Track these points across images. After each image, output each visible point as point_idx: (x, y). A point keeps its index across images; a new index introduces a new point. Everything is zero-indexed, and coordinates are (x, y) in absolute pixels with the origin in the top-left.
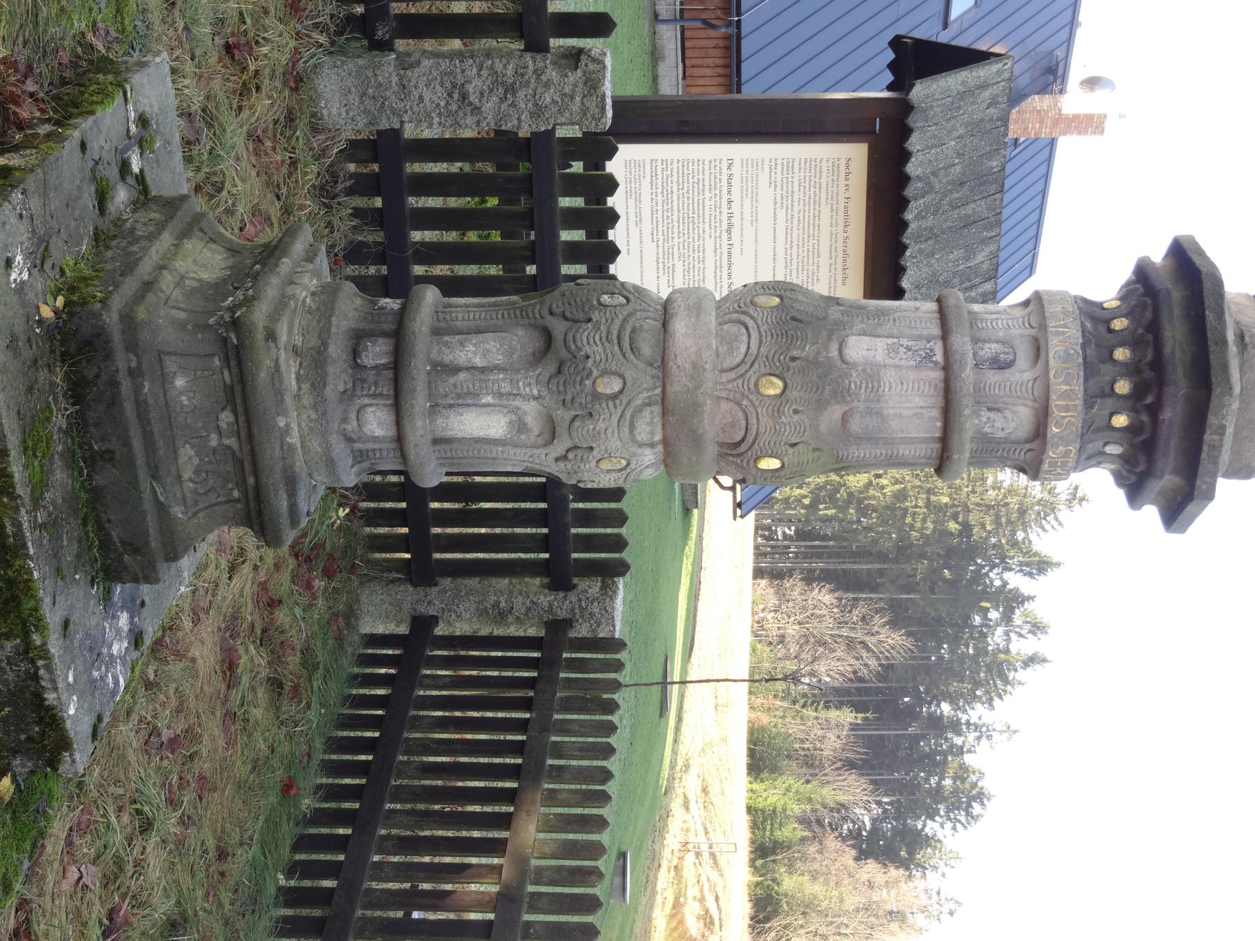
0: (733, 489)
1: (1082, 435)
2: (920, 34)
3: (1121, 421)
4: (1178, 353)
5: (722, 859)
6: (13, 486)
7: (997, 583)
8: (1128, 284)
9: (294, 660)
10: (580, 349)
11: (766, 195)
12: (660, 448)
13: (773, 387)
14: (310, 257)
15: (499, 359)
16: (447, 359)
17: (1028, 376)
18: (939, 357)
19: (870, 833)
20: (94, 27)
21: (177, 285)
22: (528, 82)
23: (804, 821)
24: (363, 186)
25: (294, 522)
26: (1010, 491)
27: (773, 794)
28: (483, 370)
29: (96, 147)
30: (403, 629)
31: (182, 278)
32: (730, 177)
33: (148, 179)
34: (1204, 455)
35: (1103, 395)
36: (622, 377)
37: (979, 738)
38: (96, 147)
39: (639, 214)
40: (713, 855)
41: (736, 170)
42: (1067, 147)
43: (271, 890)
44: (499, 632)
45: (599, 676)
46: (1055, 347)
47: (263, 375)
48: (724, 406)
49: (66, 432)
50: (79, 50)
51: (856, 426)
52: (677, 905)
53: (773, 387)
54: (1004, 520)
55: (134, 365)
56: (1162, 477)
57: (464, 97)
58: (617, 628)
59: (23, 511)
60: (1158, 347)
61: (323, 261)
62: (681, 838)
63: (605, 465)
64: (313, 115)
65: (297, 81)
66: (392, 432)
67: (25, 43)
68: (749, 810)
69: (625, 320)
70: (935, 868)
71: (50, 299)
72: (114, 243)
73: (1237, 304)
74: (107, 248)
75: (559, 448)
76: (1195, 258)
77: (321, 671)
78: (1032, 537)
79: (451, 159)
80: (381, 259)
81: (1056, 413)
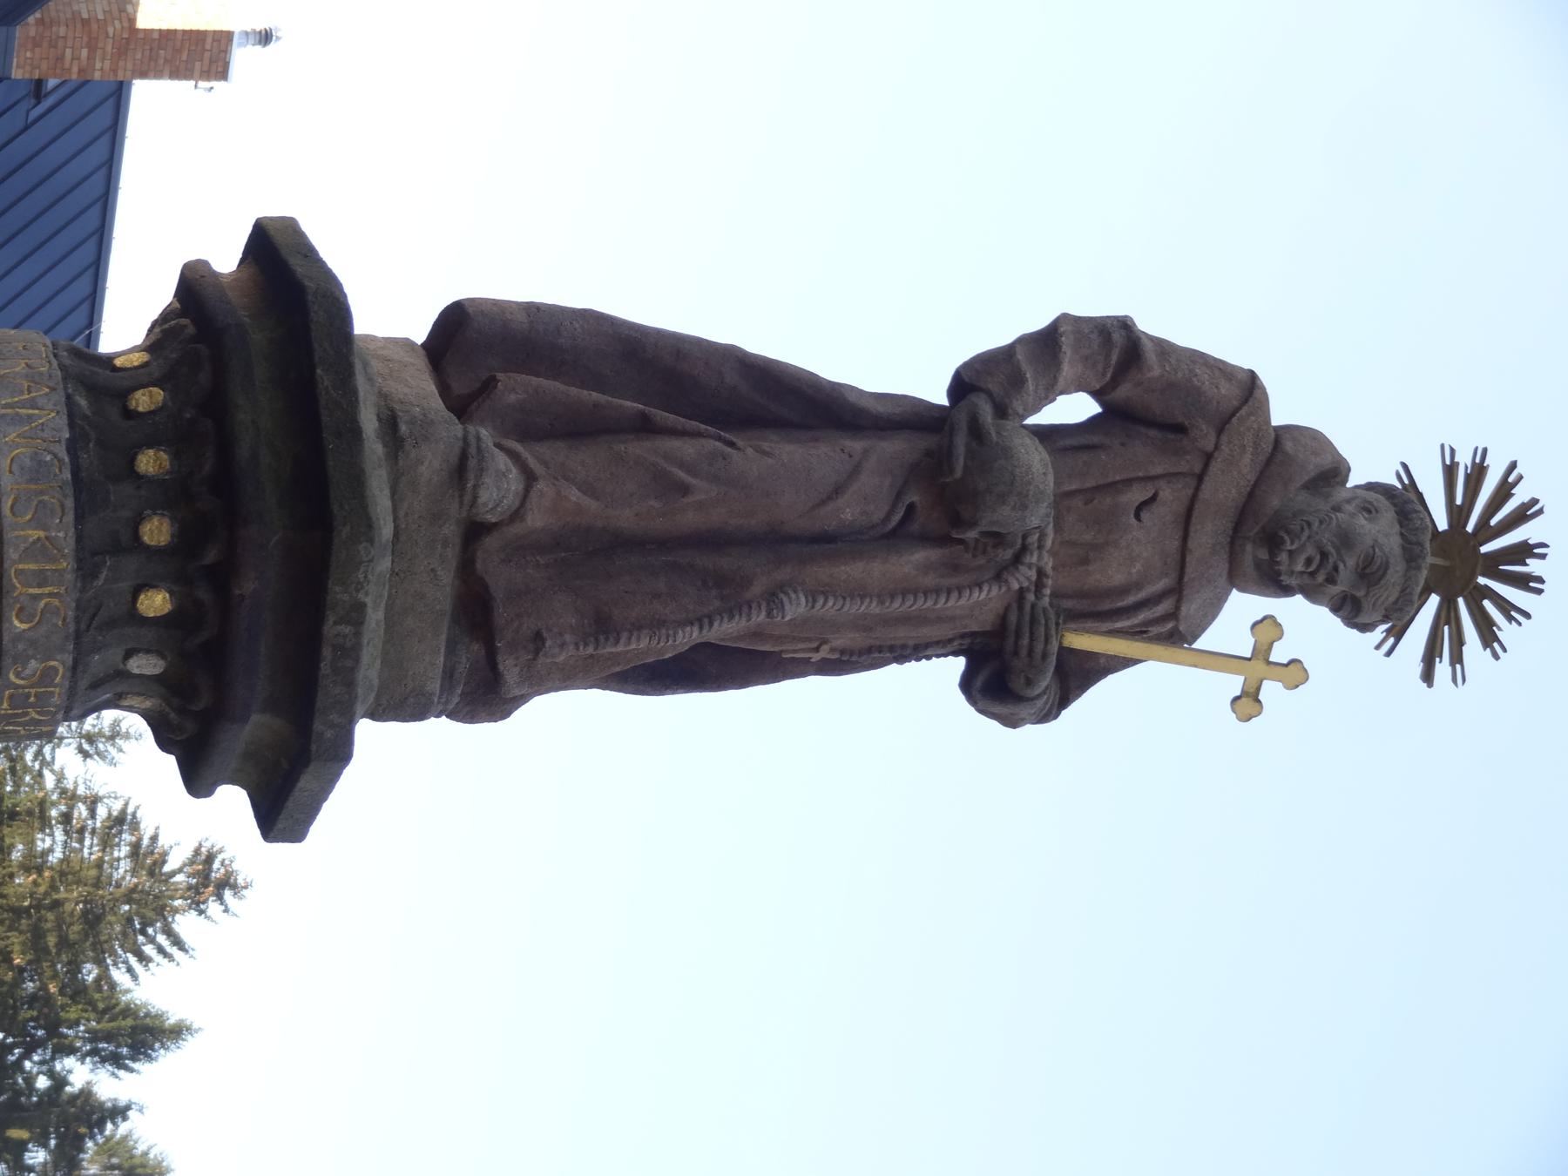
1: (78, 636)
3: (156, 603)
7: (42, 1083)
8: (166, 316)
26: (63, 874)
34: (325, 668)
35: (117, 549)
42: (150, 101)
54: (52, 940)
56: (244, 719)
73: (387, 360)
76: (296, 263)
78: (119, 975)
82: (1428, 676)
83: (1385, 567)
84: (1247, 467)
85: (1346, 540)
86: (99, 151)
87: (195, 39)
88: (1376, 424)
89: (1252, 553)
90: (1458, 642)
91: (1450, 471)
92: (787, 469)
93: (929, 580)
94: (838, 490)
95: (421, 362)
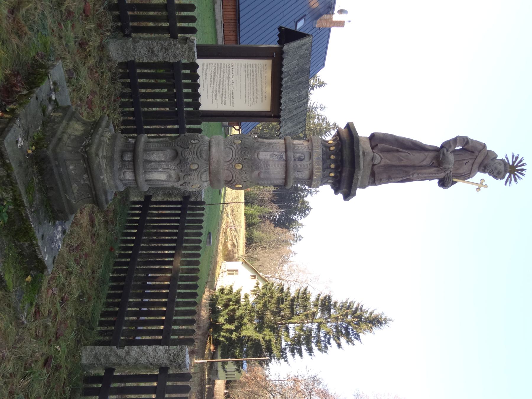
0: (239, 130)
2: (288, 27)
3: (332, 175)
4: (347, 158)
5: (238, 230)
6: (24, 204)
9: (111, 215)
10: (186, 157)
12: (209, 182)
13: (239, 167)
14: (107, 126)
15: (163, 159)
16: (148, 159)
17: (308, 163)
18: (284, 158)
19: (278, 219)
20: (37, 54)
21: (69, 138)
22: (172, 48)
23: (260, 217)
24: (123, 76)
25: (107, 203)
27: (251, 211)
28: (159, 162)
29: (41, 96)
30: (142, 199)
31: (70, 135)
32: (232, 69)
33: (58, 100)
36: (198, 164)
37: (308, 193)
38: (41, 96)
39: (206, 79)
40: (235, 229)
41: (234, 67)
43: (108, 278)
44: (170, 199)
45: (198, 212)
46: (315, 155)
47: (95, 166)
48: (226, 171)
49: (38, 183)
50: (33, 62)
51: (262, 176)
52: (225, 242)
53: (239, 167)
55: (57, 164)
57: (153, 52)
58: (203, 196)
59: (27, 210)
60: (342, 156)
61: (111, 126)
62: (226, 224)
63: (194, 187)
64: (108, 56)
65: (102, 47)
66: (133, 178)
67: (16, 65)
68: (245, 214)
69: (198, 148)
70: (296, 228)
71: (30, 148)
72: (49, 124)
74: (47, 126)
75: (181, 182)
77: (119, 215)
79: (150, 69)
80: (131, 97)
81: (315, 173)
82: (506, 184)
83: (501, 173)
84: (482, 157)
85: (496, 169)
86: (327, 37)
87: (340, 22)
88: (502, 151)
89: (482, 168)
90: (511, 180)
91: (513, 156)
92: (416, 157)
93: (435, 172)
94: (423, 161)
95: (368, 141)
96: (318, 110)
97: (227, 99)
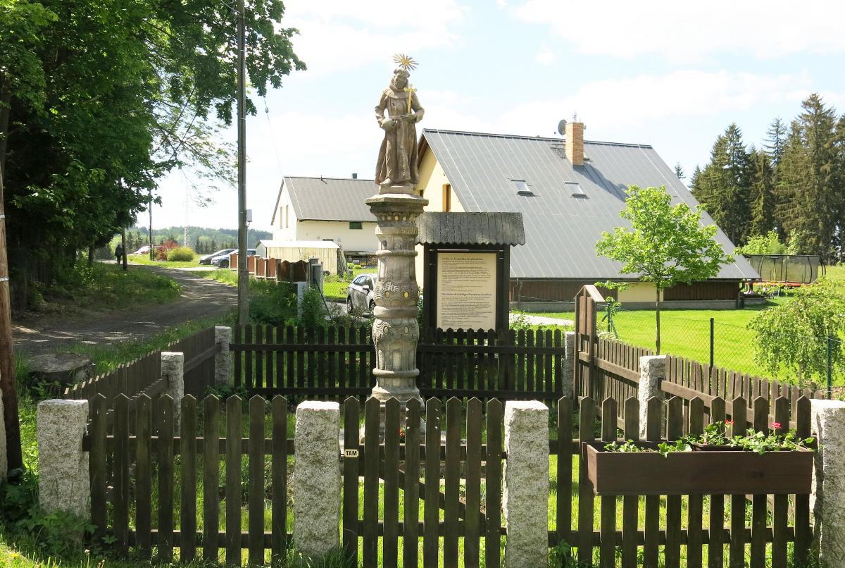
11: (453, 283)
41: (446, 293)
47: (788, 557)
96: (782, 137)
97: (483, 301)
